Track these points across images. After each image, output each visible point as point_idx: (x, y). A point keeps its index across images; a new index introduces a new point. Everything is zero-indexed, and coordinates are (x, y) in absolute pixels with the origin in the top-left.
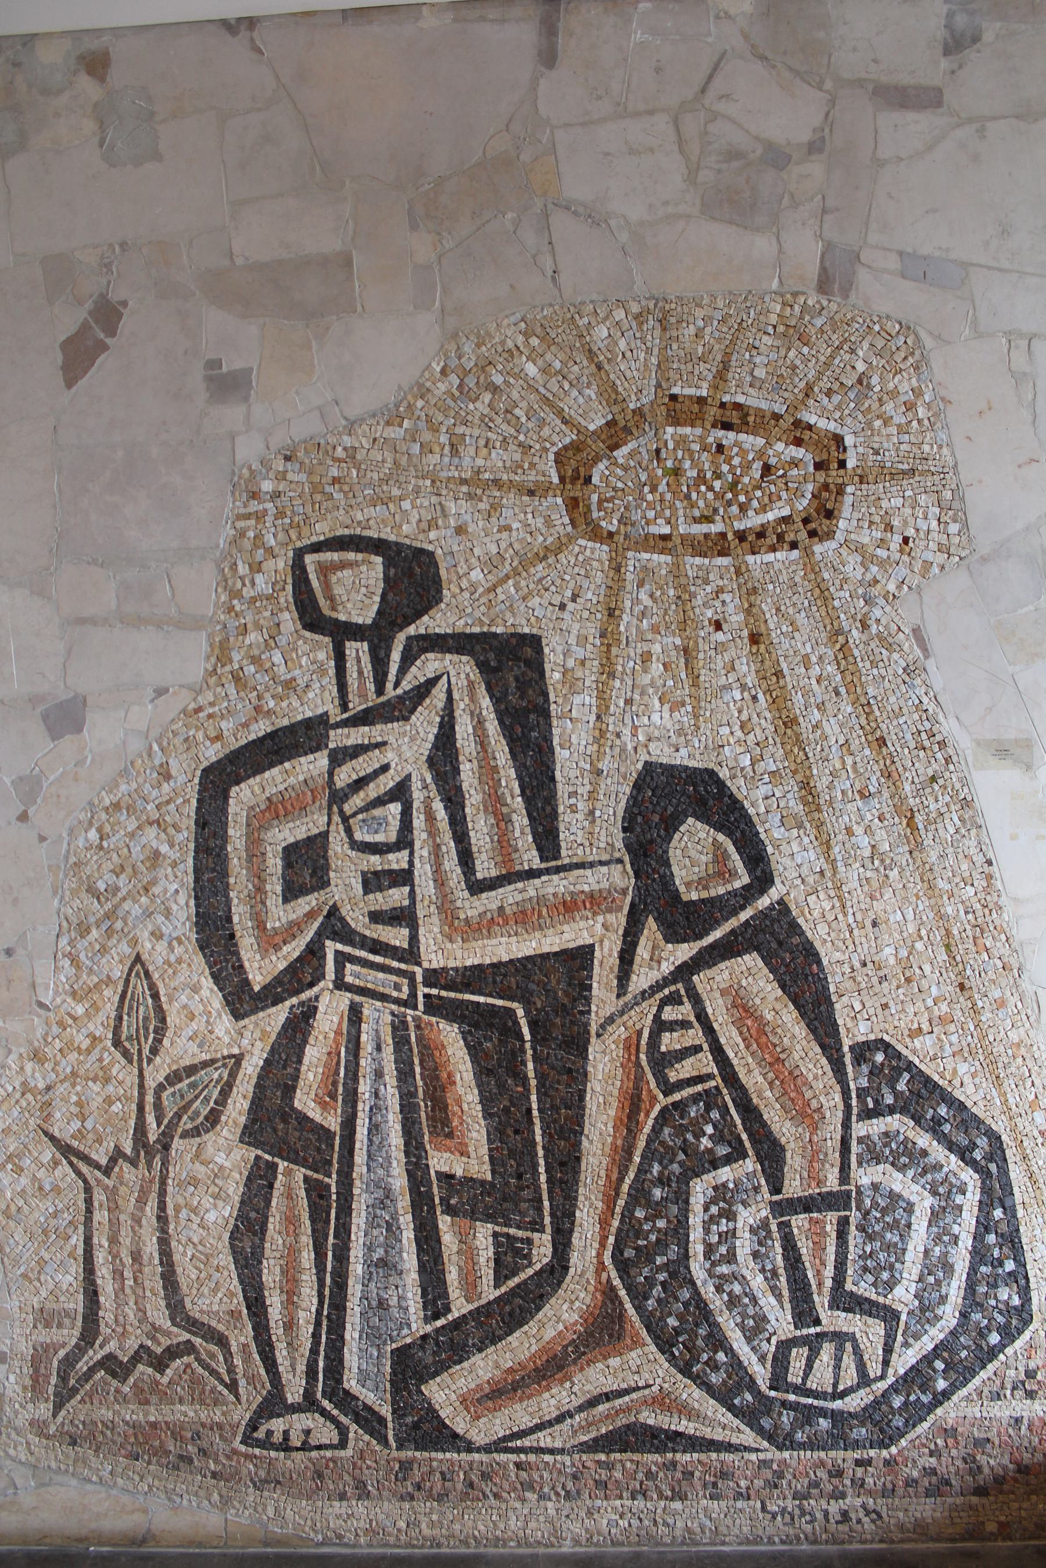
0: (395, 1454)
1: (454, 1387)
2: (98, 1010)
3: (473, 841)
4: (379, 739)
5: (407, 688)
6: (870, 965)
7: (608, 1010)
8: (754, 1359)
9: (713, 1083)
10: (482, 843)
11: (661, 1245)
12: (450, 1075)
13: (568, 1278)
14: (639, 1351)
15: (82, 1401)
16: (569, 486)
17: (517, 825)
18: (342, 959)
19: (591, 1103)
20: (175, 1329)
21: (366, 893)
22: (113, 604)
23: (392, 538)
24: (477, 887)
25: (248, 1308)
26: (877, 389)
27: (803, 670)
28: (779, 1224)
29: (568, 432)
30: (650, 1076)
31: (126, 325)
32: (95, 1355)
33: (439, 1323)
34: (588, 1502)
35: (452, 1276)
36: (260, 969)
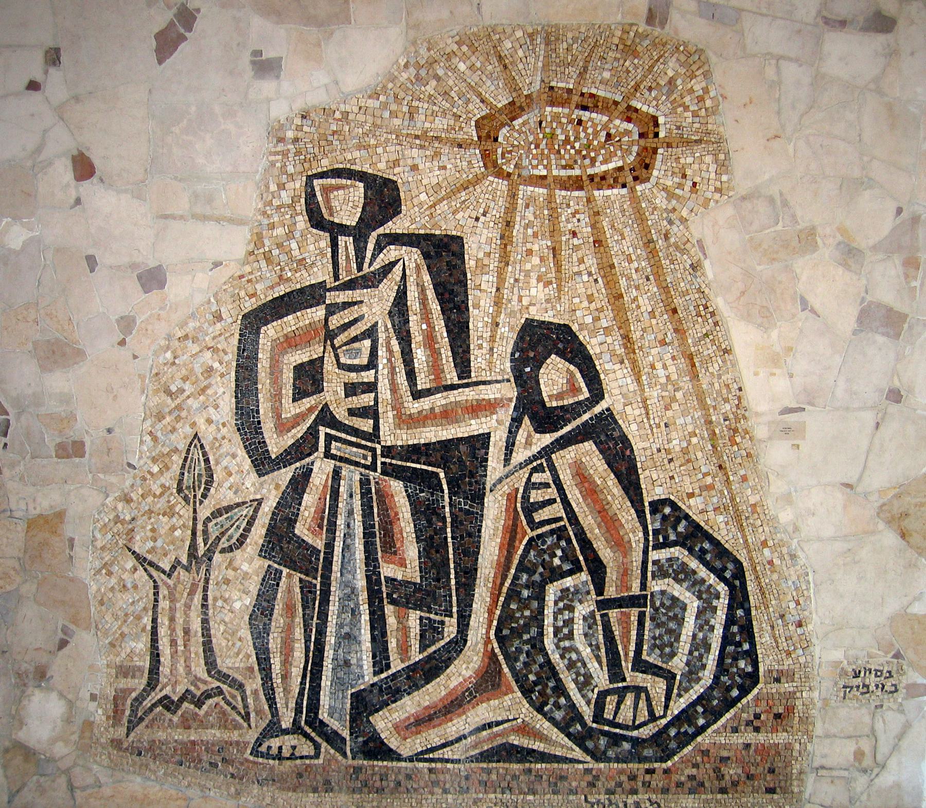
0: (350, 762)
1: (390, 719)
2: (168, 469)
3: (416, 365)
4: (359, 299)
5: (377, 267)
6: (663, 451)
7: (497, 475)
8: (583, 703)
9: (562, 523)
10: (421, 366)
11: (526, 627)
12: (397, 514)
13: (466, 648)
14: (510, 696)
15: (147, 726)
16: (483, 143)
17: (443, 356)
18: (329, 438)
19: (485, 533)
20: (210, 679)
21: (346, 397)
22: (187, 206)
23: (370, 171)
24: (417, 395)
25: (259, 664)
26: (680, 87)
27: (627, 264)
28: (602, 616)
29: (484, 108)
30: (523, 518)
31: (198, 25)
32: (156, 696)
33: (383, 676)
34: (474, 796)
35: (392, 644)
36: (276, 445)
